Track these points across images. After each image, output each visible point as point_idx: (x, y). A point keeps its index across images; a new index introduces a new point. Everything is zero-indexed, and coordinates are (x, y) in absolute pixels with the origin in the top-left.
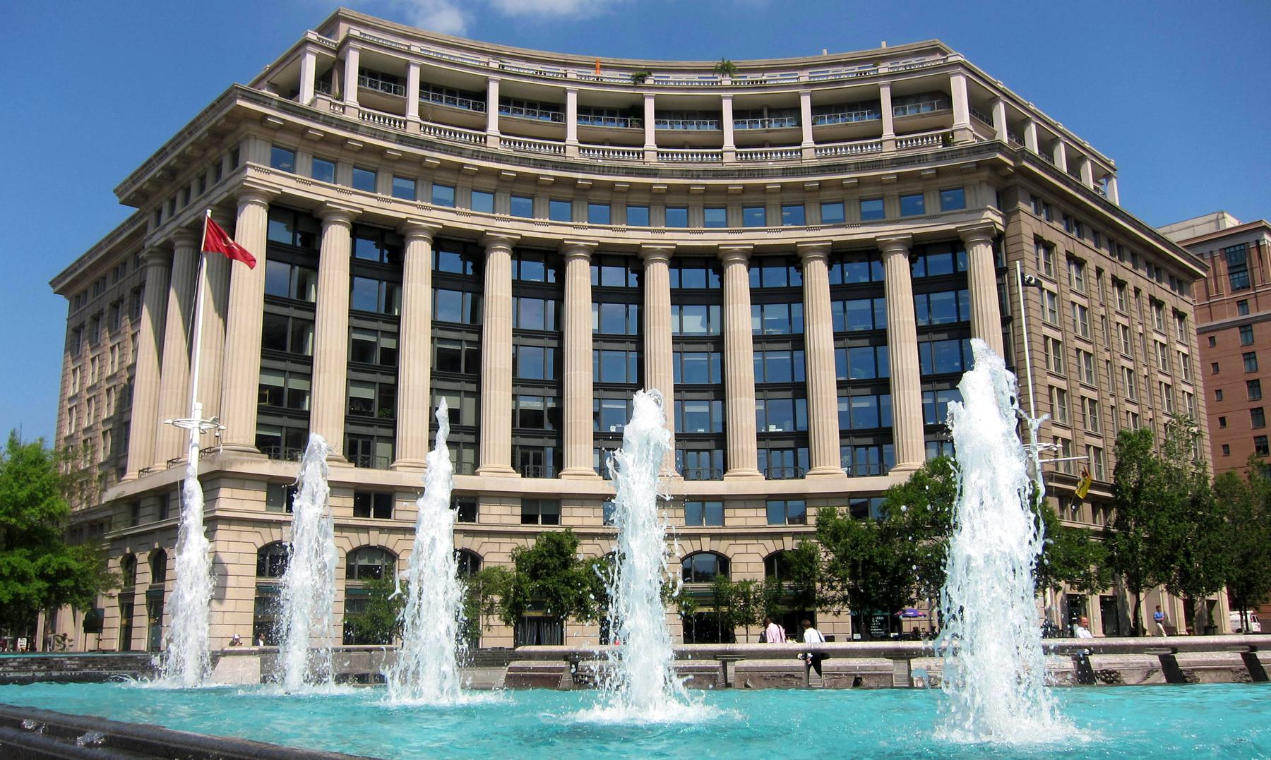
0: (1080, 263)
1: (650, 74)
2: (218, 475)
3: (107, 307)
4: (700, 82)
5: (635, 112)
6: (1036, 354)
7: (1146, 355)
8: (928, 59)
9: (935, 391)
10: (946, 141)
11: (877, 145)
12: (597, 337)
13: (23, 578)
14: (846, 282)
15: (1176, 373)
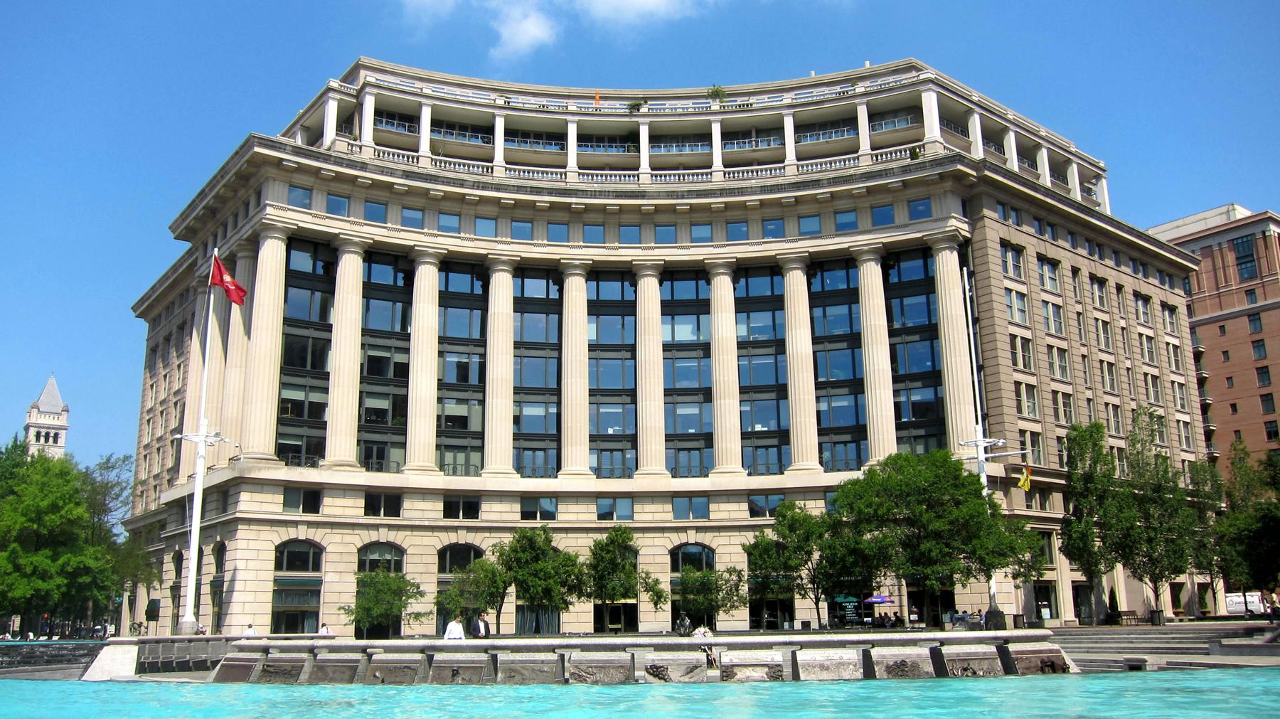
0: (1101, 282)
1: (646, 102)
2: (239, 481)
3: (175, 329)
4: (695, 108)
5: (631, 138)
8: (904, 76)
10: (914, 155)
11: (854, 160)
12: (592, 347)
13: (44, 576)
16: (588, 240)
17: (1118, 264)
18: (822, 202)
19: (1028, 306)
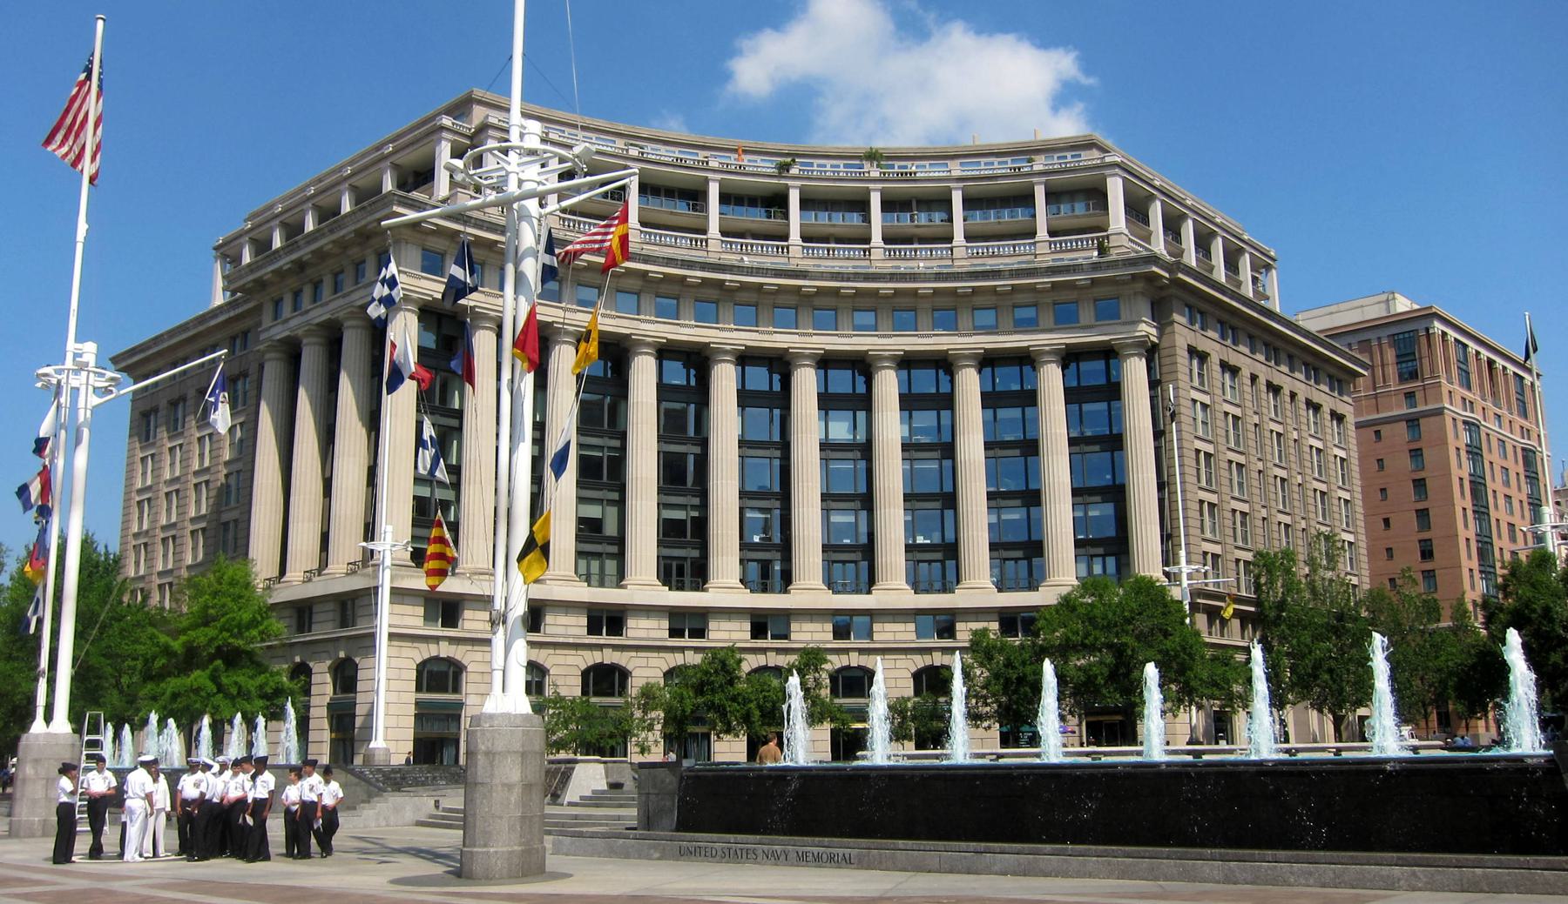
0: (1234, 371)
6: (1187, 470)
7: (1300, 464)
9: (1086, 504)
10: (1102, 250)
14: (997, 389)
15: (1333, 480)
16: (740, 322)
17: (1292, 370)
18: (1000, 295)
19: (1211, 418)
